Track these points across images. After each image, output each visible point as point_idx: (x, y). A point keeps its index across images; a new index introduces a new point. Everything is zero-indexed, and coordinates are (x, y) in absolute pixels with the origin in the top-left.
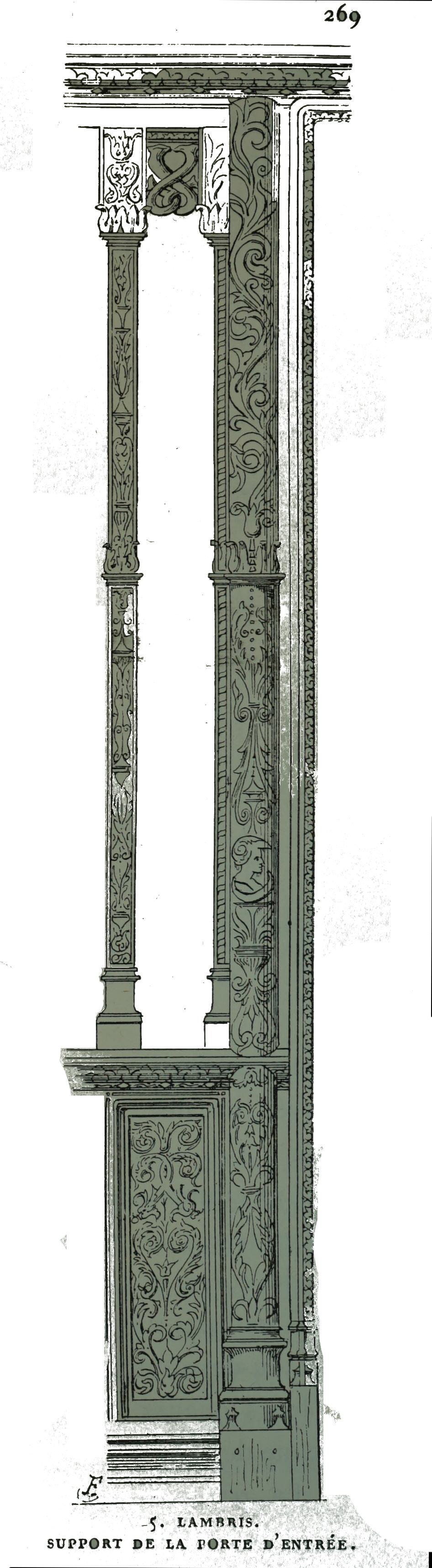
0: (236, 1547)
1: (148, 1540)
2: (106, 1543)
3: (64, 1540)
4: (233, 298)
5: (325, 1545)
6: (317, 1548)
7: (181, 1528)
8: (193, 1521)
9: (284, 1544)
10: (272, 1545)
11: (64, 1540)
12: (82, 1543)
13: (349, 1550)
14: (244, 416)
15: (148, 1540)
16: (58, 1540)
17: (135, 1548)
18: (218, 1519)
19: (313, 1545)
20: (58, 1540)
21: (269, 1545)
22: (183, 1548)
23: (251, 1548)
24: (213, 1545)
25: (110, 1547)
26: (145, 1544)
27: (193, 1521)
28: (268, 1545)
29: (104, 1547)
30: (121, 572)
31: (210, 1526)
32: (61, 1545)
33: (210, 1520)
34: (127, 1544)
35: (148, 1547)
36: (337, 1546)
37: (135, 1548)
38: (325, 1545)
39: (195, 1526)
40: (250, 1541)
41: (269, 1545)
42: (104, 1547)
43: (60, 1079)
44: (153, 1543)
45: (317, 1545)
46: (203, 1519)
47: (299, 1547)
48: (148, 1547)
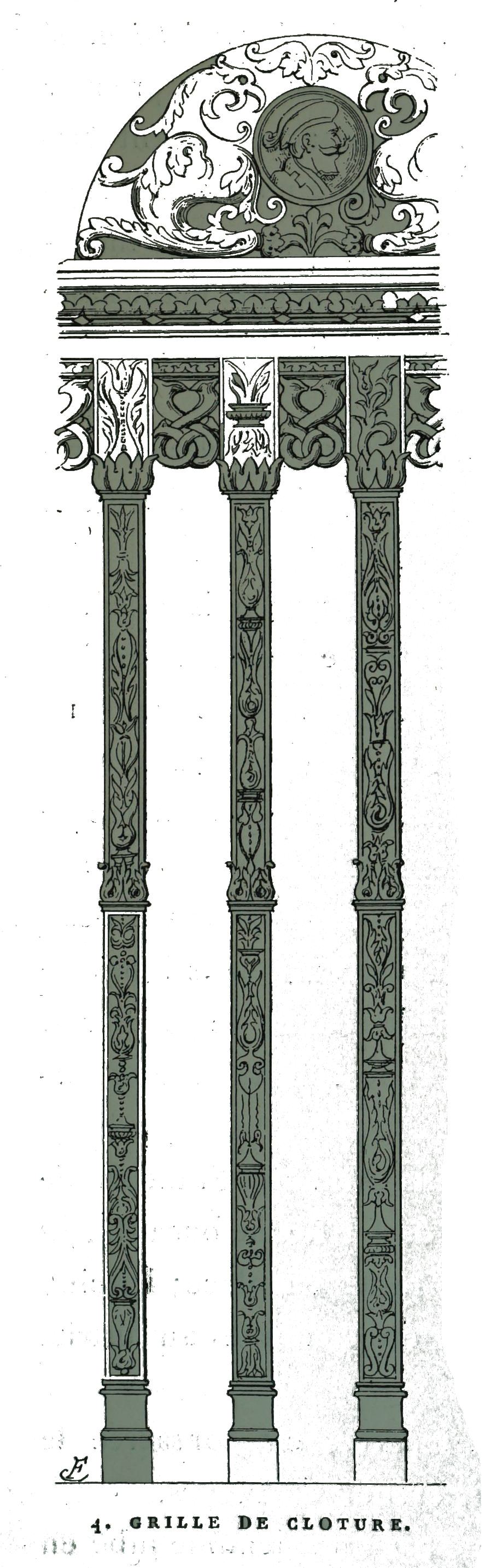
1: (259, 1519)
2: (377, 1524)
3: (364, 1520)
9: (211, 1522)
11: (364, 1520)
12: (359, 1524)
14: (306, 240)
15: (259, 1519)
16: (357, 1521)
17: (242, 1527)
19: (350, 1525)
23: (266, 1527)
26: (255, 1523)
29: (375, 1529)
30: (126, 1293)
32: (361, 1526)
34: (277, 1522)
35: (259, 1527)
37: (242, 1527)
40: (266, 1519)
43: (350, 863)
44: (218, 1522)
48: (259, 1527)
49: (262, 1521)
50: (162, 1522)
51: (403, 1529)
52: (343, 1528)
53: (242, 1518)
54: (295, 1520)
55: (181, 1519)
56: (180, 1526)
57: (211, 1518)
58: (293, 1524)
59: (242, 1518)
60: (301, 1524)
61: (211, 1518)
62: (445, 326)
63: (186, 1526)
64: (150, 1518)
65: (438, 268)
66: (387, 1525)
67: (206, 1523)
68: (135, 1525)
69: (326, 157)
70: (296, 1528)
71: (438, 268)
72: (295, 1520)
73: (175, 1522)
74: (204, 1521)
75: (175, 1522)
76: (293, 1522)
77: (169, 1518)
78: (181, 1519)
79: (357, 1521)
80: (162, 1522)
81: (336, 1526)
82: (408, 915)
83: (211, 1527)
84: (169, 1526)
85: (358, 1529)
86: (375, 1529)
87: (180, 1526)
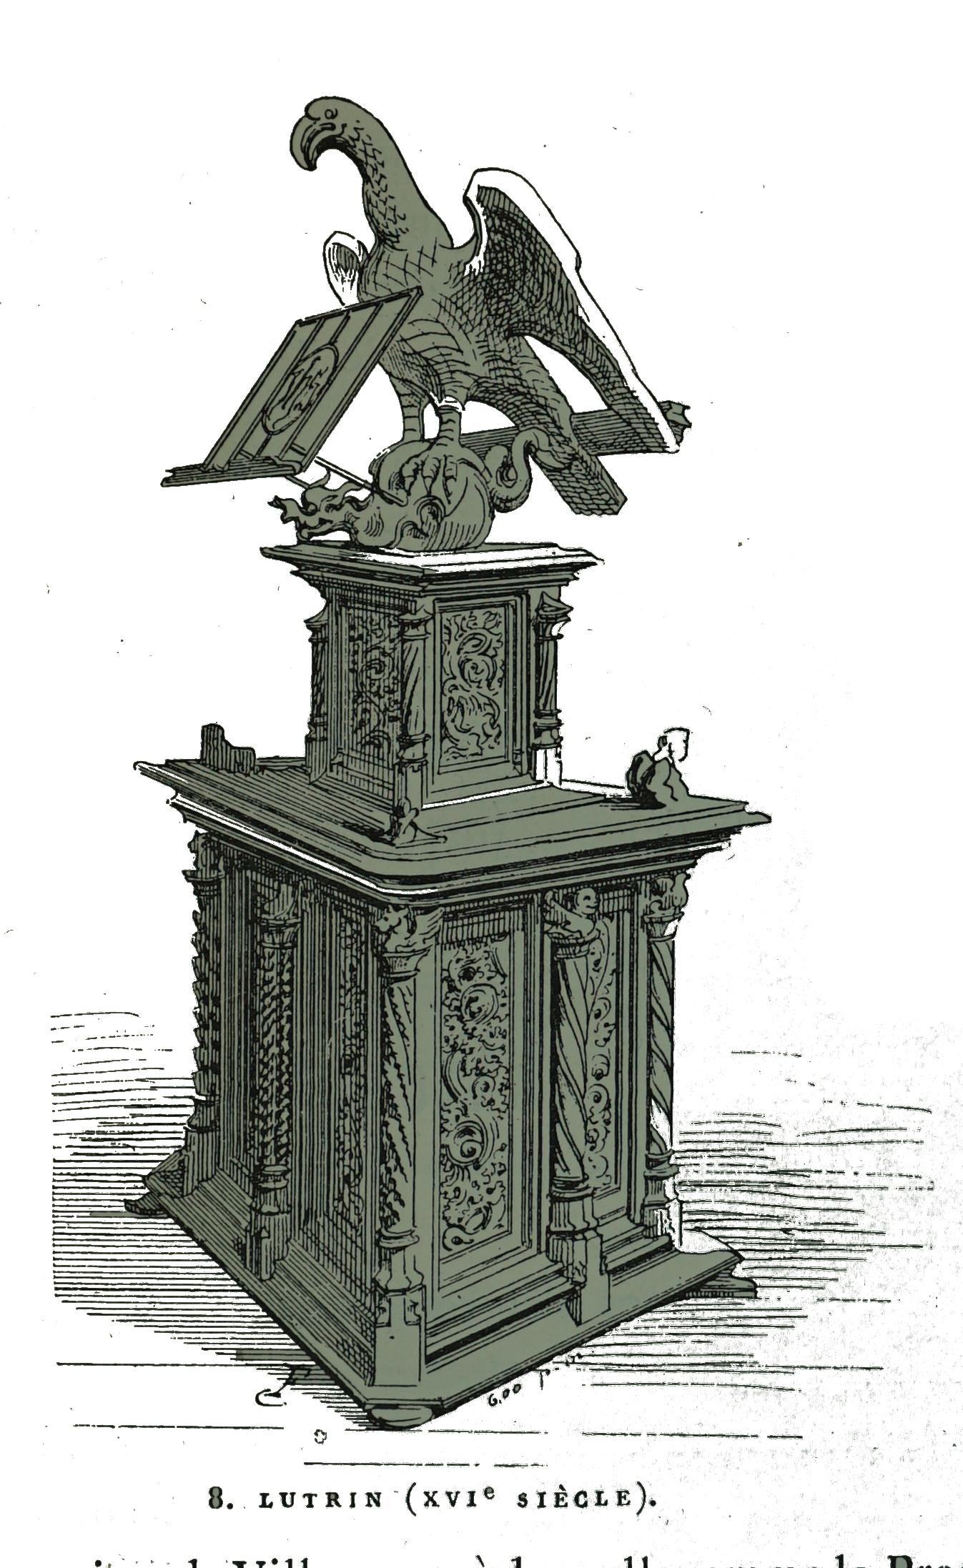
11: (293, 1494)
19: (320, 1501)
44: (628, 1497)
50: (345, 1500)
52: (310, 1505)
55: (599, 1493)
56: (599, 1503)
57: (620, 1493)
58: (582, 1500)
60: (592, 1498)
61: (620, 1493)
62: (283, 250)
63: (271, 1505)
64: (329, 1494)
67: (613, 1499)
69: (768, 819)
70: (585, 1505)
72: (585, 1494)
76: (581, 1497)
77: (542, 1495)
78: (599, 1493)
79: (283, 1495)
80: (533, 1500)
83: (557, 1505)
84: (542, 1505)
85: (285, 1504)
86: (329, 1505)
87: (599, 1503)
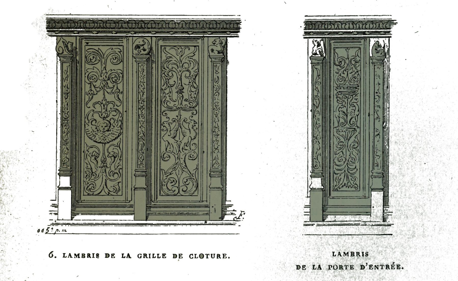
0: (346, 269)
1: (223, 254)
2: (219, 256)
3: (214, 254)
4: (403, 233)
5: (390, 267)
6: (386, 269)
7: (334, 257)
8: (339, 254)
9: (224, 256)
10: (364, 267)
11: (214, 254)
13: (401, 269)
17: (106, 257)
18: (357, 253)
20: (212, 255)
21: (363, 267)
22: (130, 257)
24: (202, 256)
25: (220, 258)
27: (339, 254)
28: (362, 267)
29: (144, 257)
31: (348, 256)
33: (348, 253)
36: (162, 257)
37: (106, 257)
38: (390, 267)
39: (341, 256)
41: (363, 267)
42: (144, 257)
45: (387, 267)
46: (75, 254)
47: (378, 268)
48: (223, 258)
49: (113, 255)
50: (91, 256)
51: (228, 258)
53: (106, 254)
54: (192, 255)
58: (191, 256)
59: (106, 254)
65: (305, 215)
66: (222, 256)
68: (139, 257)
70: (141, 257)
71: (305, 215)
72: (192, 255)
73: (151, 256)
74: (161, 255)
75: (151, 256)
81: (161, 255)
82: (230, 68)
